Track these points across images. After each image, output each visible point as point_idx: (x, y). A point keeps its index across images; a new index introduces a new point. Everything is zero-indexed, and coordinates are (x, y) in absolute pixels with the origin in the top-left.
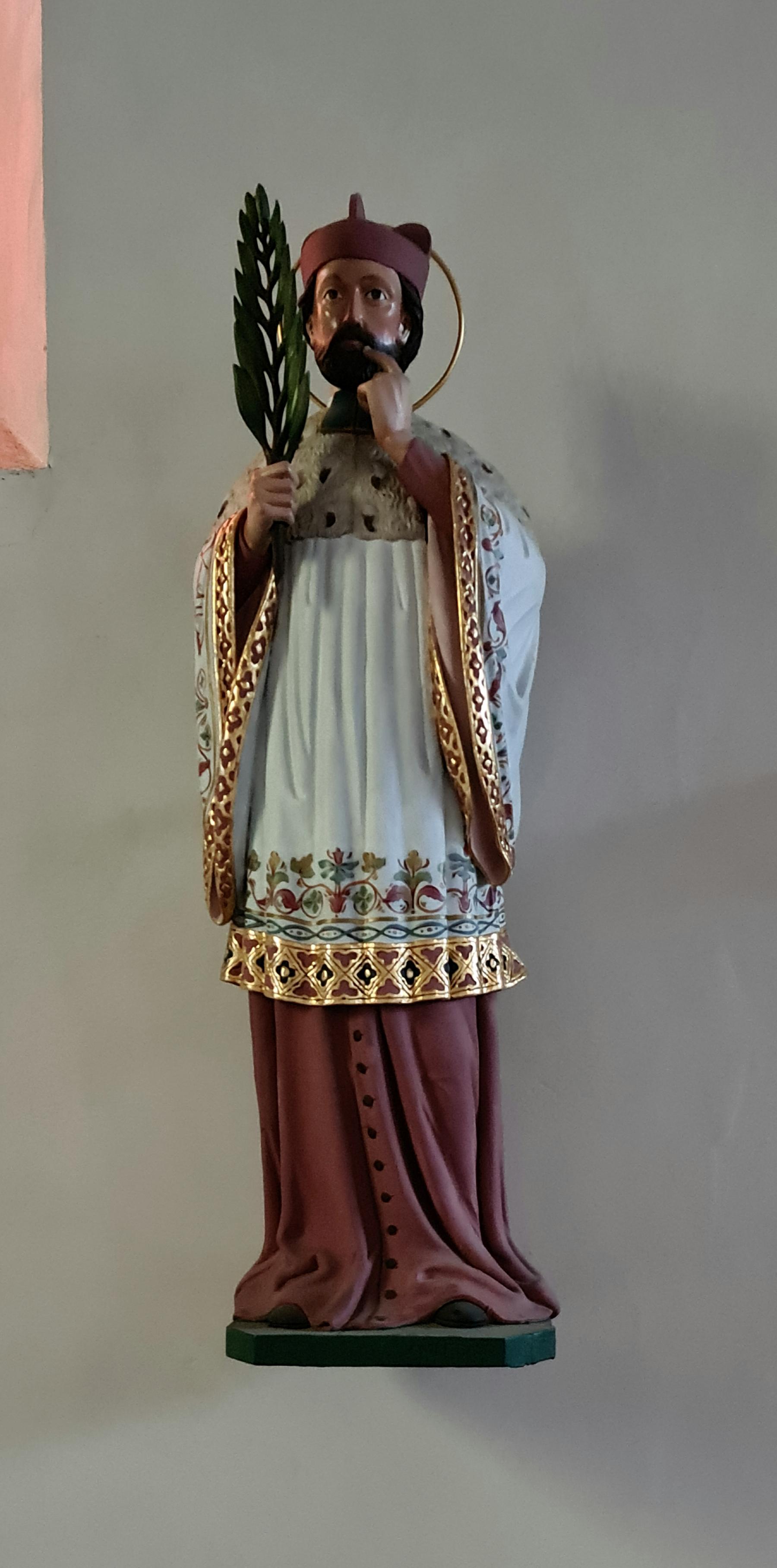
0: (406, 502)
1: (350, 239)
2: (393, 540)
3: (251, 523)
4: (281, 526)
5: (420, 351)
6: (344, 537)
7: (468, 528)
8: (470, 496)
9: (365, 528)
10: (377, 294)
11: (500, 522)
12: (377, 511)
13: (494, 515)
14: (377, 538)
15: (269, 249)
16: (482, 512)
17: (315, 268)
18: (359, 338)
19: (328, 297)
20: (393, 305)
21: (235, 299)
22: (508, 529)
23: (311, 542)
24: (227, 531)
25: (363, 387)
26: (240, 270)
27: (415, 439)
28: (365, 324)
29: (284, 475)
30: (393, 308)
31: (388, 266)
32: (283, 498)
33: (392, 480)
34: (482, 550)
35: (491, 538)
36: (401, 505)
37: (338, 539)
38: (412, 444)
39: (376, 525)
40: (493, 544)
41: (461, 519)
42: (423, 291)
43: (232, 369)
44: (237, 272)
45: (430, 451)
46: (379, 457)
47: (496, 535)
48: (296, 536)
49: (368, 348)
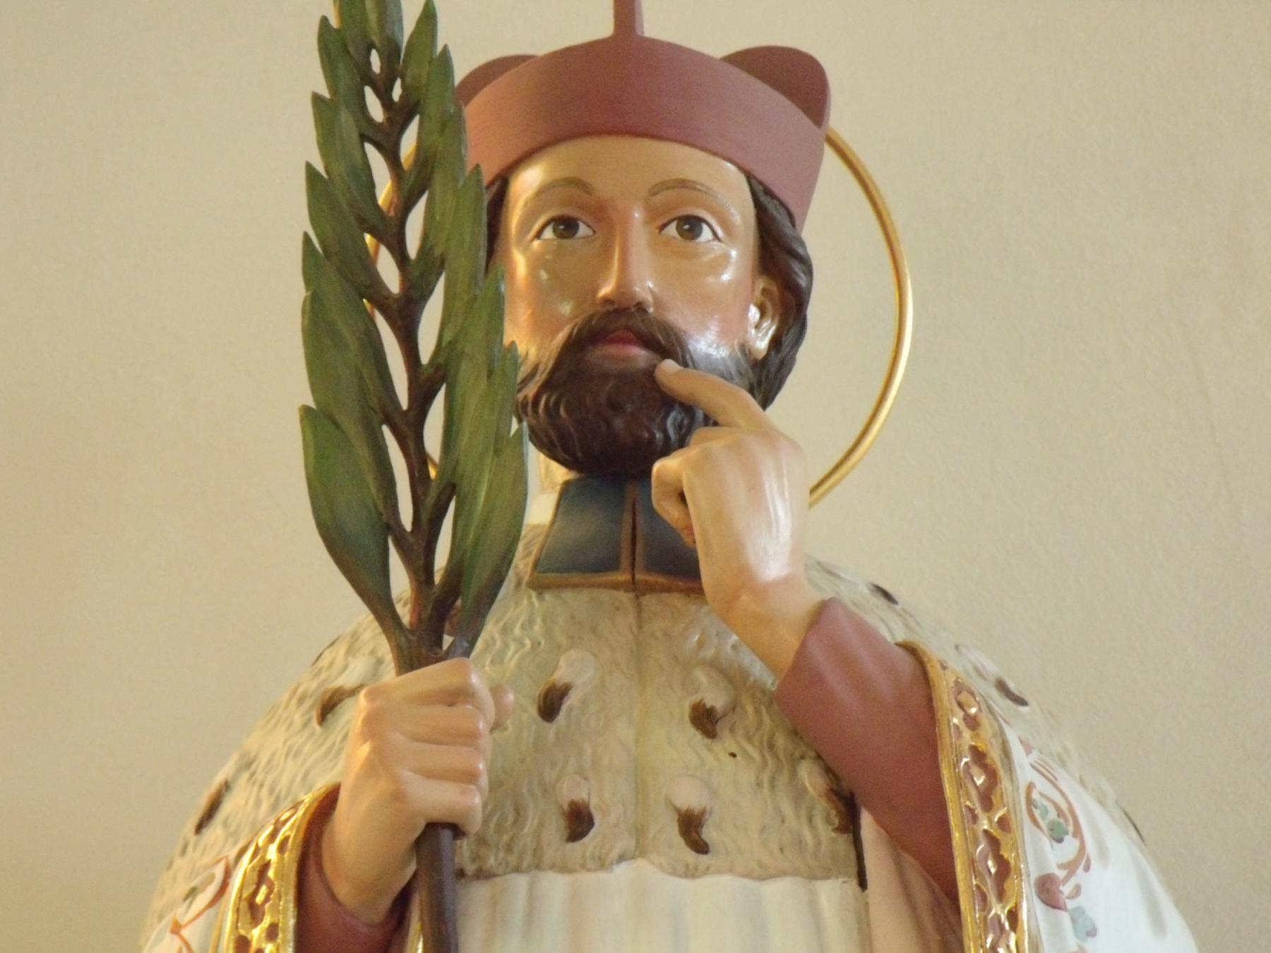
0: (794, 773)
1: (610, 89)
2: (765, 875)
3: (347, 826)
4: (446, 835)
5: (297, 292)
6: (622, 870)
7: (994, 843)
8: (995, 755)
9: (679, 841)
10: (691, 226)
11: (1078, 833)
12: (714, 793)
13: (1060, 812)
14: (719, 872)
15: (400, 115)
16: (1030, 802)
17: (513, 156)
18: (649, 342)
19: (548, 234)
20: (734, 253)
21: (306, 236)
22: (1103, 853)
23: (520, 882)
24: (272, 854)
25: (665, 467)
26: (319, 166)
27: (831, 600)
28: (658, 303)
29: (458, 696)
30: (729, 258)
31: (715, 154)
32: (456, 757)
33: (750, 709)
34: (1039, 907)
35: (1061, 874)
36: (784, 779)
37: (602, 875)
38: (821, 614)
39: (709, 833)
40: (1066, 889)
41: (975, 818)
42: (805, 214)
43: (296, 417)
44: (310, 169)
45: (868, 635)
46: (709, 653)
47: (1071, 867)
48: (470, 868)
49: (669, 365)
